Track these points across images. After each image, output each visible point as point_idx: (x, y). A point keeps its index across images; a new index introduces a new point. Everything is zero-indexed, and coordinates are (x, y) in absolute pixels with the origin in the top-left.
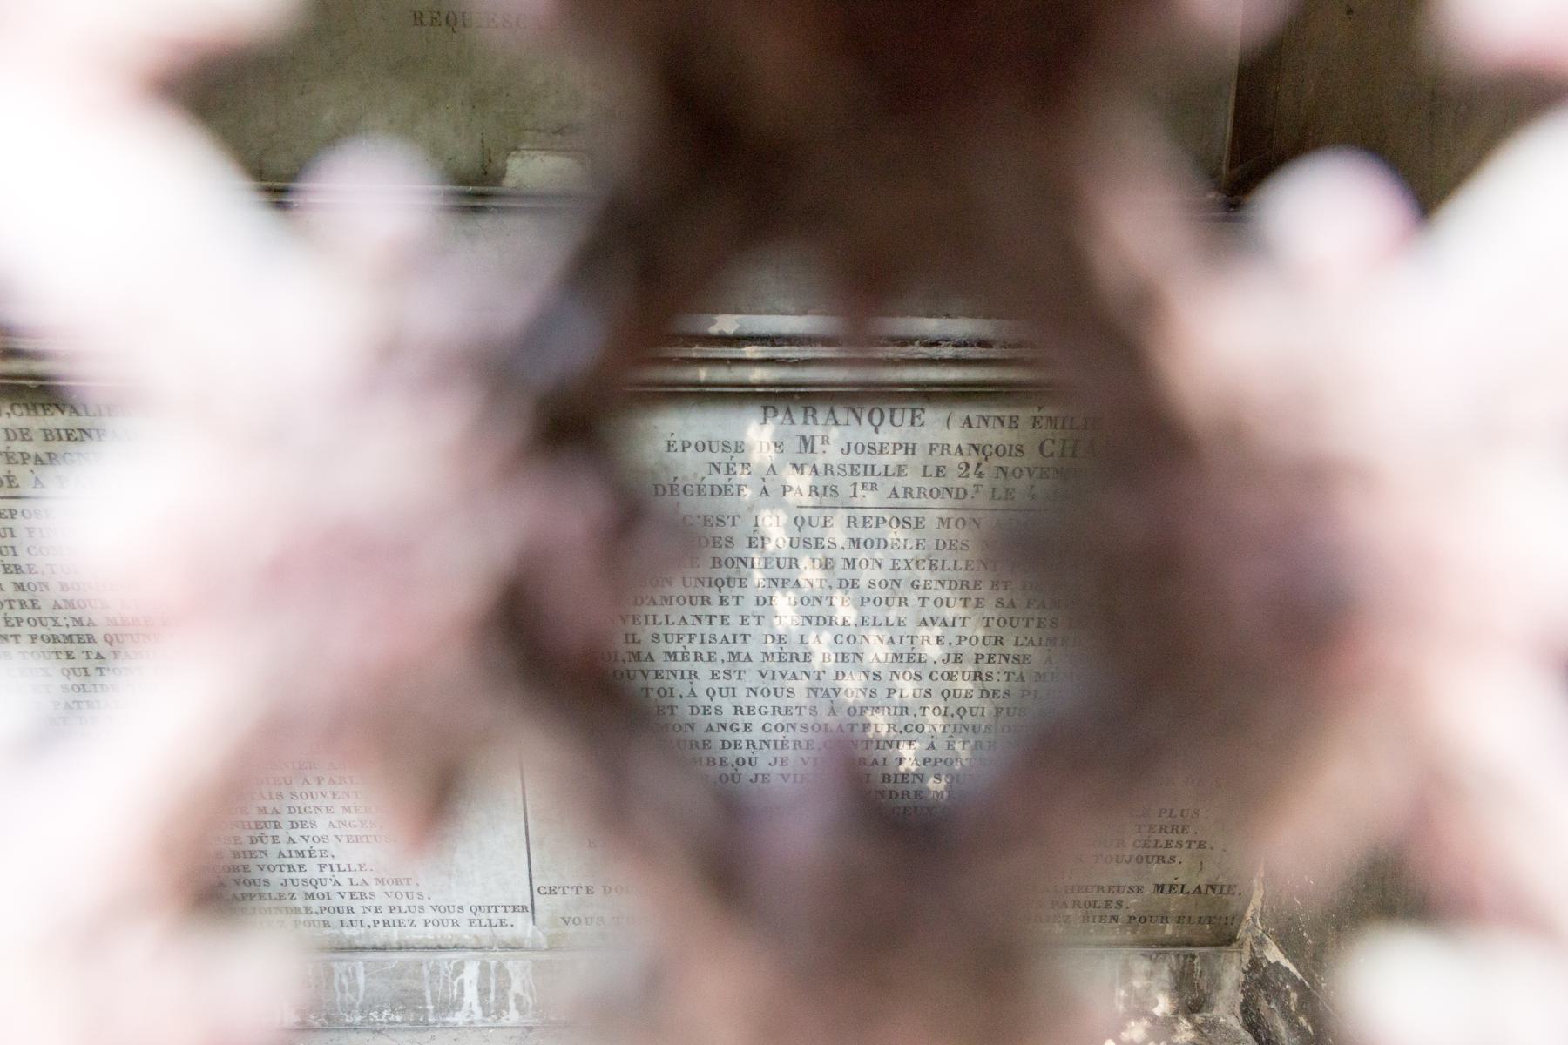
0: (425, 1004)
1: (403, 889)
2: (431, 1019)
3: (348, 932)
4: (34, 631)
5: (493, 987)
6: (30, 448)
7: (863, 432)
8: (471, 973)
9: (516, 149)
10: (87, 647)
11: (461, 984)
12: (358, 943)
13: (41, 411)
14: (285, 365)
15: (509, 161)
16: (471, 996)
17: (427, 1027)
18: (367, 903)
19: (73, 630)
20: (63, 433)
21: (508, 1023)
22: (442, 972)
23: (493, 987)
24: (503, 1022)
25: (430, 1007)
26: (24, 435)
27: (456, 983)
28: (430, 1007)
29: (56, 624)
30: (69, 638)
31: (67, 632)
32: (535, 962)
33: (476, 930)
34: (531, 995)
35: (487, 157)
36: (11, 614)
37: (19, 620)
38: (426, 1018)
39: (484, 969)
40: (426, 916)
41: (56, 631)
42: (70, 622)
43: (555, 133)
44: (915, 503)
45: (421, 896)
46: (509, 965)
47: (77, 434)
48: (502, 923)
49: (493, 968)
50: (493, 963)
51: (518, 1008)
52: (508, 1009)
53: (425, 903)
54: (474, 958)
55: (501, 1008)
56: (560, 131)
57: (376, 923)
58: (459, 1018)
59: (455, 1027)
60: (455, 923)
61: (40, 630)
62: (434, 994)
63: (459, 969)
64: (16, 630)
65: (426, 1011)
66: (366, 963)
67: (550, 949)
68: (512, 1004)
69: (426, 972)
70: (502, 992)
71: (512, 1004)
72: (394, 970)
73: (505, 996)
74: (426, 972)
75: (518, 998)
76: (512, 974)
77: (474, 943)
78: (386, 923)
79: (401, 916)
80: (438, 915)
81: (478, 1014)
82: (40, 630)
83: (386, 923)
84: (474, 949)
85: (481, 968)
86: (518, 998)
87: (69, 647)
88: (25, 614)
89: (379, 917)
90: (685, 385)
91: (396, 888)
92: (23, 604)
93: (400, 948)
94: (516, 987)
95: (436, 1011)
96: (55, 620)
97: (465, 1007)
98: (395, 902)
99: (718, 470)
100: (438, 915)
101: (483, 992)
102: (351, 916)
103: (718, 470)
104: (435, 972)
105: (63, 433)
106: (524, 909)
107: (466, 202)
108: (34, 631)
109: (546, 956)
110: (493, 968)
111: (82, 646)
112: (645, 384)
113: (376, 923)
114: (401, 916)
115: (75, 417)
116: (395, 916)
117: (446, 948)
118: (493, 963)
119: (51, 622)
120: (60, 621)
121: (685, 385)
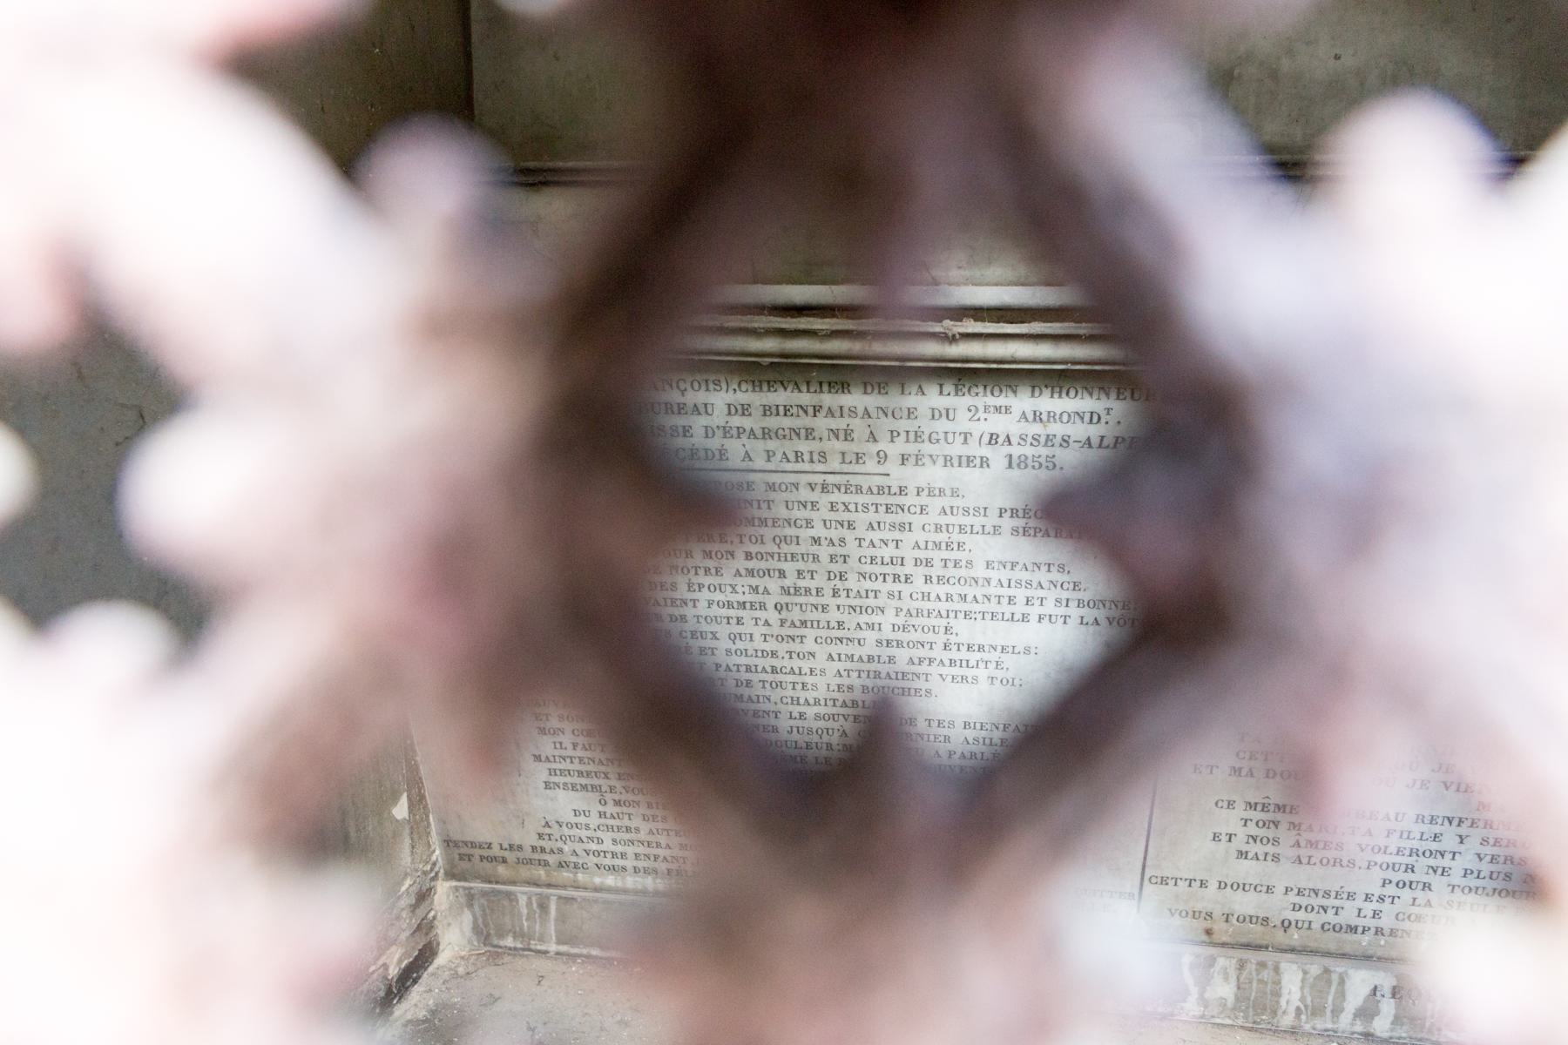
6: (747, 423)
7: (745, 396)
10: (758, 614)
13: (765, 387)
14: (328, 344)
19: (749, 598)
20: (781, 409)
26: (745, 410)
29: (734, 591)
30: (743, 605)
31: (741, 598)
37: (700, 586)
41: (733, 598)
42: (747, 589)
44: (806, 466)
47: (794, 410)
87: (741, 613)
90: (720, 354)
99: (798, 435)
103: (798, 435)
105: (781, 409)
107: (523, 179)
111: (185, 607)
112: (710, 353)
115: (796, 393)
119: (729, 589)
121: (720, 354)
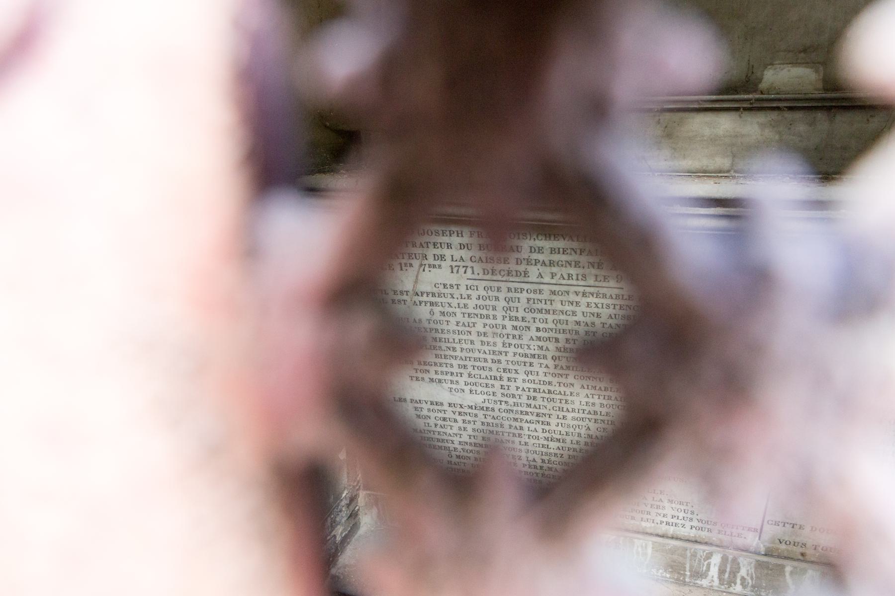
0: (685, 571)
1: (683, 507)
2: (687, 580)
3: (644, 524)
4: (516, 350)
5: (728, 570)
6: (541, 257)
8: (716, 560)
9: (772, 64)
10: (542, 361)
11: (709, 565)
12: (649, 531)
13: (552, 238)
15: (765, 72)
16: (714, 572)
17: (684, 583)
18: (660, 511)
21: (734, 591)
22: (698, 556)
23: (728, 570)
24: (731, 590)
25: (688, 573)
27: (706, 563)
28: (688, 573)
31: (533, 352)
32: (757, 561)
33: (720, 536)
34: (752, 578)
35: (751, 69)
36: (507, 341)
37: (510, 345)
38: (684, 579)
39: (724, 559)
40: (693, 524)
41: (528, 352)
42: (536, 348)
43: (800, 52)
45: (692, 513)
46: (741, 560)
48: (739, 535)
49: (730, 559)
50: (730, 557)
51: (742, 584)
52: (735, 584)
53: (694, 517)
54: (719, 552)
55: (731, 582)
56: (805, 51)
57: (662, 522)
58: (705, 582)
59: (701, 587)
60: (709, 530)
61: (520, 351)
62: (691, 567)
63: (709, 556)
64: (507, 349)
65: (685, 575)
66: (654, 543)
67: (766, 555)
68: (738, 581)
69: (689, 555)
70: (734, 573)
71: (738, 581)
72: (670, 550)
73: (735, 576)
74: (689, 555)
75: (743, 579)
76: (741, 565)
77: (718, 543)
78: (668, 523)
79: (678, 521)
80: (700, 525)
81: (716, 582)
82: (520, 351)
83: (668, 523)
84: (717, 546)
85: (722, 558)
86: (743, 579)
87: (532, 360)
88: (514, 342)
89: (665, 520)
91: (678, 506)
92: (514, 337)
93: (696, 542)
94: (743, 572)
95: (691, 576)
96: (529, 346)
97: (709, 578)
98: (676, 514)
100: (700, 525)
101: (722, 572)
102: (649, 517)
104: (694, 555)
106: (755, 530)
108: (516, 350)
109: (765, 559)
110: (730, 559)
113: (662, 522)
114: (678, 521)
116: (675, 520)
117: (700, 543)
118: (730, 557)
119: (526, 347)
120: (531, 347)
